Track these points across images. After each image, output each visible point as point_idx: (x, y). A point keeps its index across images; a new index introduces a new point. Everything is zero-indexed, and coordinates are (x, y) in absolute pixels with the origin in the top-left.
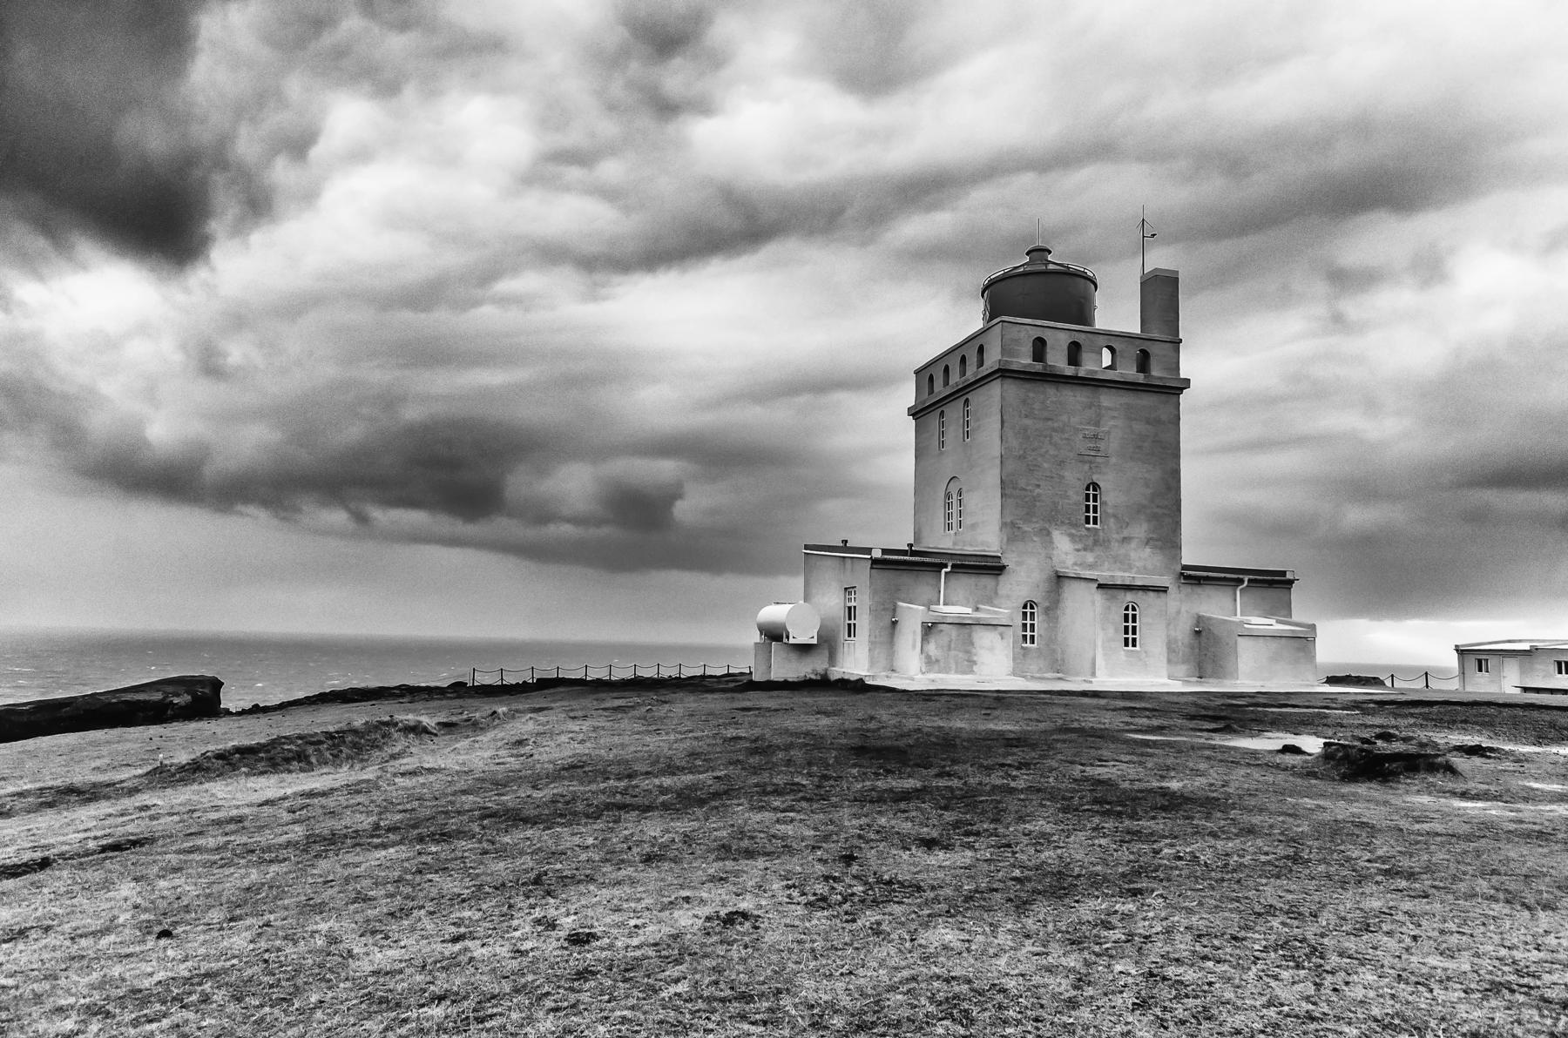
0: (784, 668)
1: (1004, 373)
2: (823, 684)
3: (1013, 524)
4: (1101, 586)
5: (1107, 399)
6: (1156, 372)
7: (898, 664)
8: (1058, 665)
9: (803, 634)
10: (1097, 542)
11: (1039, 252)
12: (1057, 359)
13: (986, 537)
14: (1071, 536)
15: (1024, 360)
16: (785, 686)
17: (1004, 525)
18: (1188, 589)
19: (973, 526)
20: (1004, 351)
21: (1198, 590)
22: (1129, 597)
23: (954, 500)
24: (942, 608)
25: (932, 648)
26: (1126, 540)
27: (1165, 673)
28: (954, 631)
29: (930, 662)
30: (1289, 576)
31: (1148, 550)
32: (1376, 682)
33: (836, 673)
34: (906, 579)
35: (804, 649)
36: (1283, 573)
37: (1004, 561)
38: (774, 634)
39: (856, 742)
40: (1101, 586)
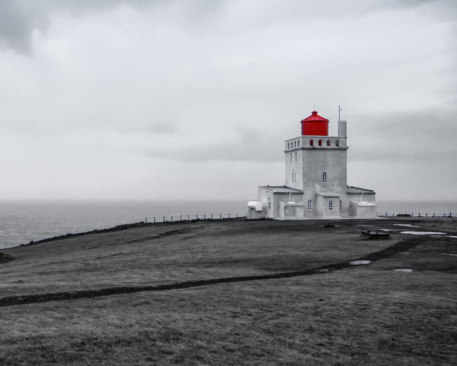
0: (254, 216)
1: (303, 149)
2: (264, 219)
3: (306, 183)
4: (324, 197)
5: (328, 153)
6: (341, 145)
7: (280, 215)
8: (279, 216)
9: (258, 209)
10: (325, 186)
11: (315, 113)
12: (316, 145)
13: (300, 186)
14: (320, 185)
15: (308, 146)
16: (255, 220)
17: (303, 183)
18: (349, 196)
19: (298, 183)
20: (303, 144)
21: (351, 196)
22: (330, 199)
23: (294, 175)
24: (290, 203)
25: (287, 211)
26: (333, 185)
27: (339, 215)
28: (291, 208)
29: (286, 214)
30: (374, 192)
31: (338, 187)
32: (409, 216)
33: (267, 217)
34: (281, 196)
35: (260, 212)
36: (373, 191)
37: (304, 191)
38: (252, 209)
39: (327, 332)
40: (324, 197)
